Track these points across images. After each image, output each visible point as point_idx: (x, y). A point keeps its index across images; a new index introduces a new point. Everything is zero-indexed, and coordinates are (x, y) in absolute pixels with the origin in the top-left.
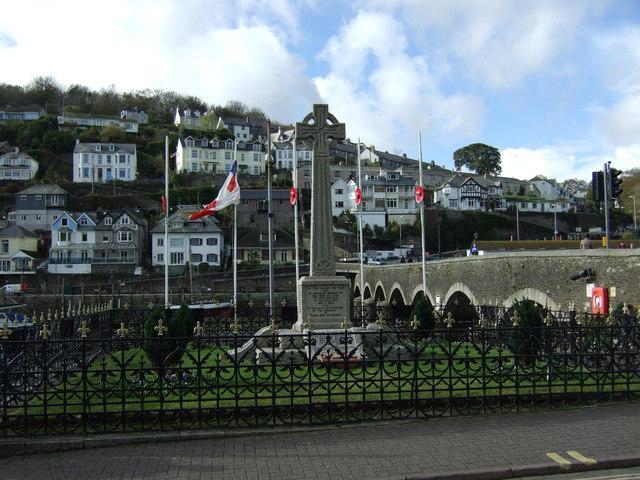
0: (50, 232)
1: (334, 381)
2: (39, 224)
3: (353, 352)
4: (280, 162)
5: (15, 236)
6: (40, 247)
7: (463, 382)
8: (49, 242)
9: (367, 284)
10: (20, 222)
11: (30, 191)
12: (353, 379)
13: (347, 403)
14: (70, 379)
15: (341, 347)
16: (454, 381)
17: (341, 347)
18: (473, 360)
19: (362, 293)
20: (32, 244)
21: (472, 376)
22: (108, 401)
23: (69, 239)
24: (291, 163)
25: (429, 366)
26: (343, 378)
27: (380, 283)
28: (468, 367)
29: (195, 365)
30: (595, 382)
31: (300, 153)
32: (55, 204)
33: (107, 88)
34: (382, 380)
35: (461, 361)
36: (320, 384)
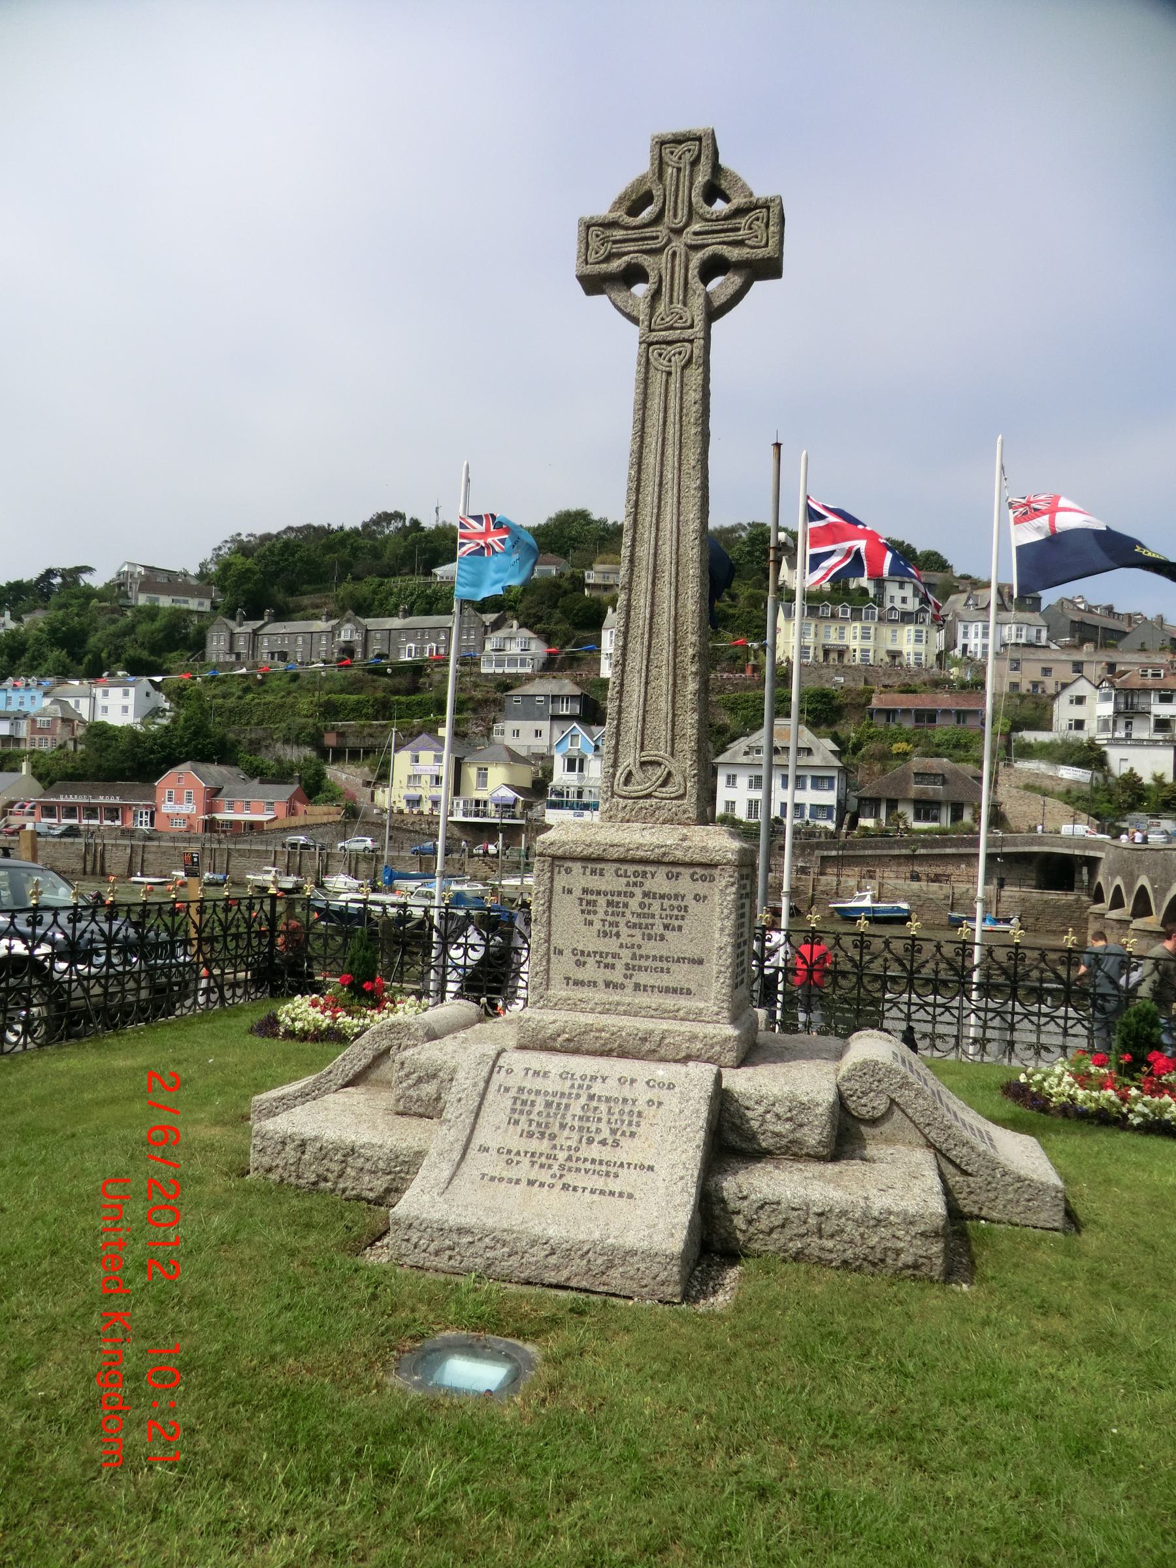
0: (552, 757)
1: (1046, 1015)
2: (540, 745)
3: (923, 965)
4: (965, 647)
5: (497, 761)
6: (535, 783)
7: (1031, 1021)
8: (549, 774)
9: (1119, 881)
10: (509, 741)
11: (529, 689)
12: (918, 1001)
13: (10, 939)
14: (842, 982)
15: (1062, 970)
16: (1070, 1023)
17: (1062, 970)
18: (844, 974)
19: (1108, 896)
20: (525, 777)
21: (1046, 1015)
22: (939, 1019)
23: (581, 770)
24: (985, 646)
25: (461, 951)
26: (955, 1003)
27: (1143, 881)
28: (465, 954)
29: (483, 942)
30: (929, 1018)
31: (1006, 629)
32: (565, 712)
33: (19, 579)
34: (909, 1004)
35: (876, 977)
36: (1026, 1016)
